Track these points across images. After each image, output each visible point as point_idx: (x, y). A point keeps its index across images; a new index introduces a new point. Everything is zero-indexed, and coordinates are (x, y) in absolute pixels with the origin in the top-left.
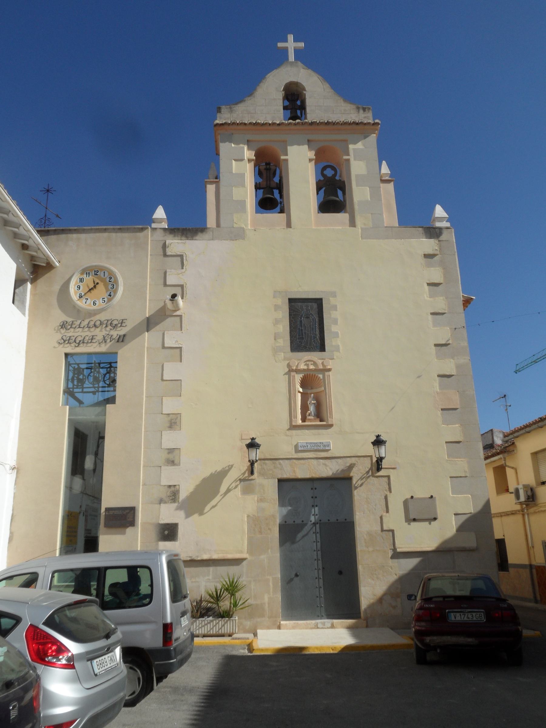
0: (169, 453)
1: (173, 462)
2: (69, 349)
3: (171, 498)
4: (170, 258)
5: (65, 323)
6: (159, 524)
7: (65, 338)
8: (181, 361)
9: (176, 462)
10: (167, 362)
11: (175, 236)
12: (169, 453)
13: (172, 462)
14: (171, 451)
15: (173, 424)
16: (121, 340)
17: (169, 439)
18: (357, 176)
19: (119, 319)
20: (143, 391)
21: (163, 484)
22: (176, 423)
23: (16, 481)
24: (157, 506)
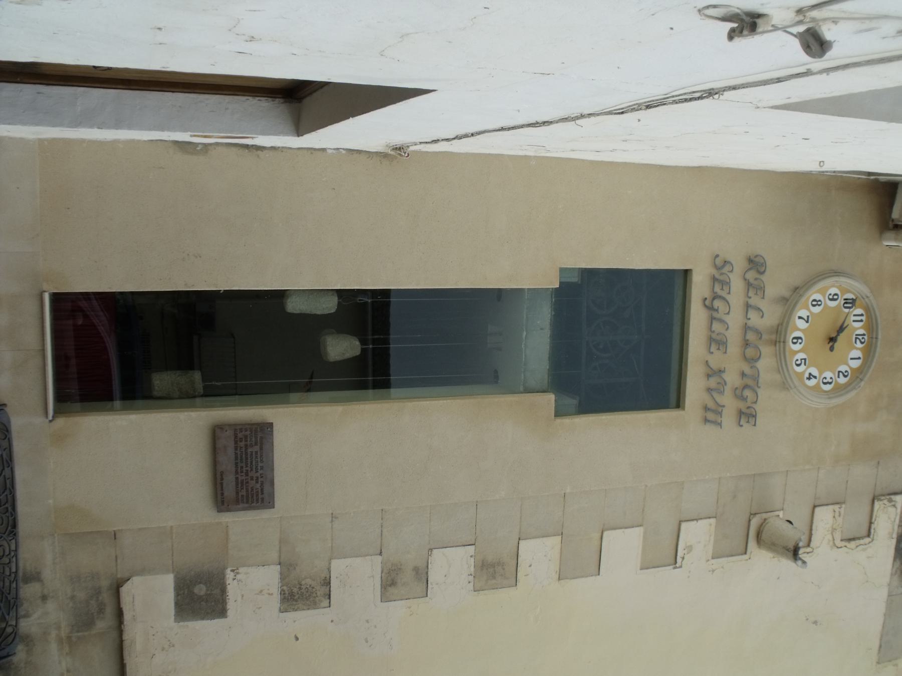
0: (416, 570)
1: (393, 583)
2: (699, 288)
3: (295, 590)
4: (867, 509)
5: (762, 270)
6: (225, 568)
7: (727, 268)
8: (641, 569)
9: (391, 590)
10: (645, 533)
11: (285, 102)
12: (416, 570)
13: (390, 583)
14: (422, 575)
15: (491, 570)
16: (711, 416)
17: (451, 567)
18: (264, 430)
19: (757, 407)
20: (45, 145)
21: (335, 564)
22: (494, 578)
23: (359, 152)
24: (275, 556)
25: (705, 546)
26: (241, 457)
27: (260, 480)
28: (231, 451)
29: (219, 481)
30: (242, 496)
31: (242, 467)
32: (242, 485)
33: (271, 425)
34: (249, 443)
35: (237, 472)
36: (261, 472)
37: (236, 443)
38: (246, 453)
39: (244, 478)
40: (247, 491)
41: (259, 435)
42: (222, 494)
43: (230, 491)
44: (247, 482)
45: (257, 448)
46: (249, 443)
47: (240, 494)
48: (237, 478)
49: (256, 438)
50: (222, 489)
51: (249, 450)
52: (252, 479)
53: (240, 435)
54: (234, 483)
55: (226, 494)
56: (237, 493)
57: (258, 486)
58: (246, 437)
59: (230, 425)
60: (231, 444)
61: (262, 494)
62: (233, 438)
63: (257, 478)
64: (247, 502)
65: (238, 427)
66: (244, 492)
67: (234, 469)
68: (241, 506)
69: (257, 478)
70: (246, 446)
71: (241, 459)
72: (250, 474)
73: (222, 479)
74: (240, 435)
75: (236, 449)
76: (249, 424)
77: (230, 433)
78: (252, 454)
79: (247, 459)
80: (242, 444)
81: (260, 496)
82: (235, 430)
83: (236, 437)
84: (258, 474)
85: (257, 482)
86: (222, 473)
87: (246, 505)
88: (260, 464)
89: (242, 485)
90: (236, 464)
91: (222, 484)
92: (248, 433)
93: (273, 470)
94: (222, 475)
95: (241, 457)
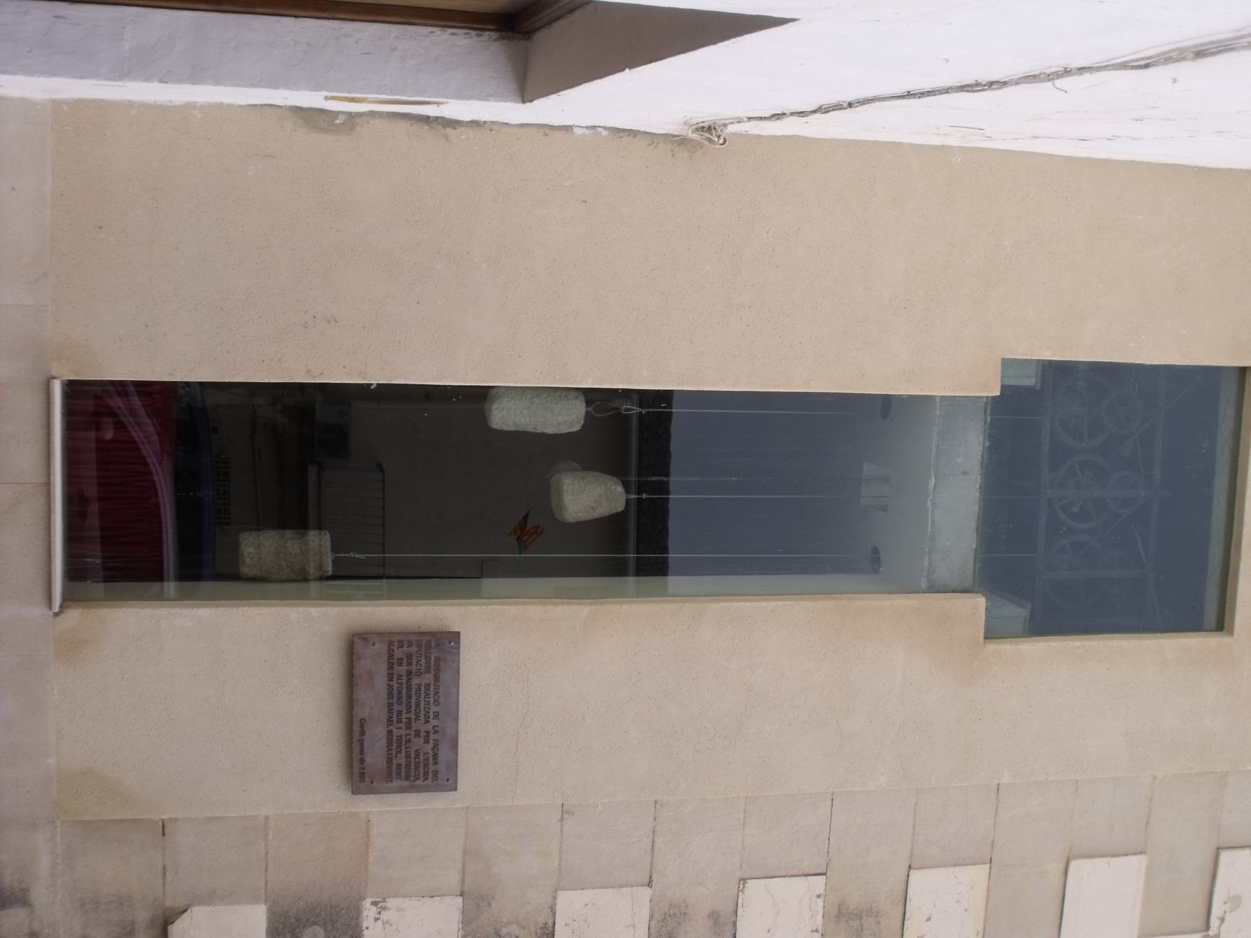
18: (440, 648)
26: (400, 692)
27: (432, 737)
28: (381, 682)
29: (356, 736)
30: (399, 765)
31: (400, 713)
32: (399, 745)
37: (391, 666)
38: (409, 689)
39: (402, 732)
40: (408, 756)
42: (362, 761)
43: (376, 755)
44: (409, 741)
45: (429, 678)
46: (414, 667)
47: (395, 762)
48: (390, 732)
49: (428, 659)
50: (362, 752)
51: (415, 681)
52: (418, 734)
53: (399, 653)
54: (384, 742)
55: (369, 759)
56: (389, 760)
57: (429, 748)
58: (409, 656)
59: (380, 634)
60: (382, 669)
61: (436, 763)
62: (386, 658)
63: (428, 733)
64: (407, 778)
66: (402, 760)
67: (384, 716)
68: (396, 783)
69: (428, 733)
70: (409, 673)
71: (400, 698)
72: (415, 726)
73: (363, 733)
74: (399, 653)
77: (380, 647)
78: (419, 690)
79: (409, 697)
80: (403, 669)
81: (432, 768)
82: (391, 643)
83: (391, 656)
84: (429, 727)
85: (427, 741)
86: (363, 722)
87: (406, 783)
88: (434, 708)
89: (399, 745)
91: (361, 742)
92: (414, 649)
93: (456, 720)
94: (362, 726)
95: (400, 692)
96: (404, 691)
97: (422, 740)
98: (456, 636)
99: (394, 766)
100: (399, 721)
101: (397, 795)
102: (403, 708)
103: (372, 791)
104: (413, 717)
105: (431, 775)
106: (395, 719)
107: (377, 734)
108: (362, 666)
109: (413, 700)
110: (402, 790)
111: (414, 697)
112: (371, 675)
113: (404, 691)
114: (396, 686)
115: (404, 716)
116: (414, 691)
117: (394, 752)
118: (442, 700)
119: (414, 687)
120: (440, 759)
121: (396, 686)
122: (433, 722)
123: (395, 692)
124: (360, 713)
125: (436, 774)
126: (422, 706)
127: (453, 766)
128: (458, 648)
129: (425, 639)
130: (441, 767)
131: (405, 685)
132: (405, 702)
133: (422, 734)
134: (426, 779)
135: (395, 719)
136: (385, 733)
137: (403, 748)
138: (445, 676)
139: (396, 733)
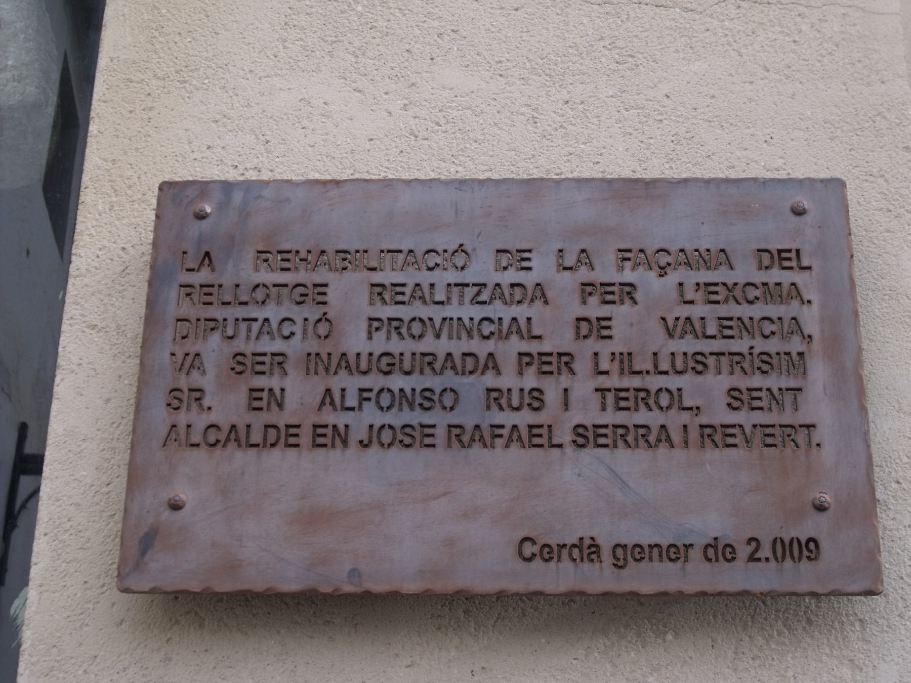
18: (199, 233)
25: (641, 604)
26: (404, 399)
27: (606, 271)
28: (346, 477)
29: (600, 578)
30: (736, 398)
31: (495, 397)
32: (644, 397)
33: (171, 192)
34: (295, 348)
35: (537, 437)
36: (542, 268)
37: (287, 437)
38: (389, 364)
39: (583, 386)
40: (698, 364)
41: (243, 270)
42: (719, 551)
43: (694, 495)
44: (625, 362)
45: (348, 293)
46: (295, 348)
47: (722, 415)
48: (585, 437)
49: (263, 293)
50: (675, 553)
51: (356, 341)
52: (600, 328)
53: (227, 406)
54: (628, 462)
55: (710, 522)
56: (715, 436)
57: (648, 281)
58: (240, 364)
59: (135, 479)
60: (289, 472)
61: (724, 258)
62: (240, 458)
63: (587, 289)
64: (797, 363)
65: (160, 416)
66: (710, 391)
67: (511, 460)
68: (819, 406)
69: (587, 289)
70: (315, 363)
71: (427, 399)
72: (558, 339)
73: (589, 550)
74: (227, 406)
75: (327, 437)
76: (147, 344)
77: (194, 480)
78: (395, 325)
79: (428, 361)
80: (299, 392)
81: (745, 271)
82: (175, 437)
83: (235, 437)
84: (564, 285)
85: (629, 291)
86: (536, 550)
87: (819, 373)
88: (482, 269)
89: (644, 397)
90: (458, 436)
91: (627, 554)
92: (214, 349)
93: (533, 187)
94: (623, 369)
95: (404, 399)
96: (397, 382)
97: (621, 313)
98: (171, 192)
99: (743, 417)
100: (537, 394)
101: (876, 405)
102: (471, 387)
103: (862, 506)
104: (516, 345)
105: (775, 275)
106: (524, 418)
107: (586, 491)
108: (274, 557)
109: (442, 346)
110: (852, 388)
111: (427, 344)
112: (312, 518)
113: (397, 382)
114: (371, 415)
115: (508, 380)
116: (396, 346)
117: (675, 420)
118: (446, 241)
119: (380, 343)
120: (707, 239)
121: (371, 415)
122: (542, 268)
123: (395, 418)
124: (490, 564)
125: (783, 257)
126: (469, 312)
127: (735, 195)
128: (227, 187)
129: (174, 304)
130: (742, 237)
131: (374, 381)
132: (449, 379)
133: (594, 309)
134: (795, 290)
135: (524, 418)
136: (588, 454)
137: (654, 382)
138: (342, 228)
139: (588, 412)
